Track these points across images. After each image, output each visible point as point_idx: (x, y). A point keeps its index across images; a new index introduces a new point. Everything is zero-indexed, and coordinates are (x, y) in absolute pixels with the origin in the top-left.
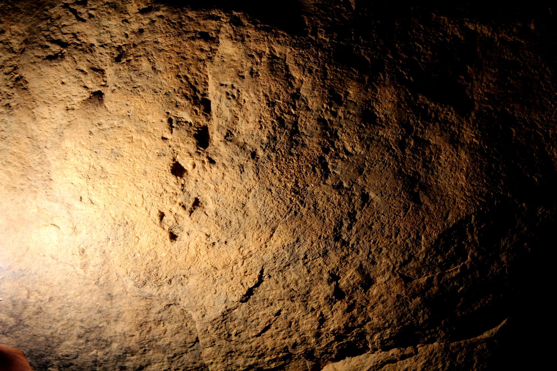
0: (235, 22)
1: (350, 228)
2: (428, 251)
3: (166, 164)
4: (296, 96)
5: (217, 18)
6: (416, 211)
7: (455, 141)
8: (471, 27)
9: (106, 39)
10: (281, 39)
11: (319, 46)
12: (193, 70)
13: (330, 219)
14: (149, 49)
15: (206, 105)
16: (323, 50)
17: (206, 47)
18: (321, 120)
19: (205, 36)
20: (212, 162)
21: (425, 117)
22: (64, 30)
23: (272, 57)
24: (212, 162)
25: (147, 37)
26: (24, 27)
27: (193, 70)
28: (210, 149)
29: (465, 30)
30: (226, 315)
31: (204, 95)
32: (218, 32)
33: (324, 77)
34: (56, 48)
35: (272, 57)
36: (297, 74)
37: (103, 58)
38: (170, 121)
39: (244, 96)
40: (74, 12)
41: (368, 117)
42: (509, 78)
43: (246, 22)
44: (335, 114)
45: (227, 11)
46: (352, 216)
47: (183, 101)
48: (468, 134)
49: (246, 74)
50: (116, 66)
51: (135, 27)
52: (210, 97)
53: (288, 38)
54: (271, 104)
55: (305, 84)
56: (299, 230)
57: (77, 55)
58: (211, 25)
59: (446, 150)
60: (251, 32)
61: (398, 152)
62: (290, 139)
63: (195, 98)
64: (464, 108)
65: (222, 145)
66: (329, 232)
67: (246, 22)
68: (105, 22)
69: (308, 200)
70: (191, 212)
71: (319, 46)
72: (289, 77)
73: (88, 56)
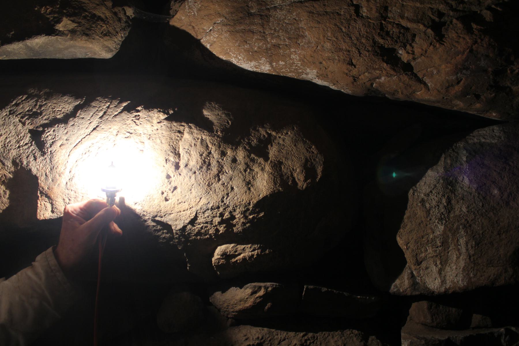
0: (190, 128)
1: (227, 198)
2: (253, 207)
3: (164, 175)
4: (210, 153)
5: (184, 126)
6: (249, 194)
7: (263, 170)
8: (269, 132)
9: (146, 132)
10: (205, 134)
11: (218, 136)
12: (175, 143)
13: (220, 196)
14: (160, 135)
15: (179, 155)
16: (220, 138)
17: (179, 135)
18: (218, 162)
19: (179, 132)
20: (180, 174)
21: (253, 160)
22: (131, 128)
23: (202, 139)
24: (180, 174)
25: (159, 131)
26: (118, 127)
27: (175, 143)
28: (180, 170)
29: (267, 133)
30: (185, 227)
31: (178, 152)
32: (184, 130)
33: (220, 147)
34: (128, 134)
35: (202, 139)
36: (210, 146)
37: (145, 138)
38: (166, 160)
39: (192, 152)
40: (135, 122)
41: (234, 160)
42: (188, 268)
43: (193, 127)
44: (223, 160)
45: (187, 123)
46: (228, 194)
47: (171, 154)
48: (268, 168)
49: (193, 145)
50: (149, 141)
51: (156, 128)
52: (180, 153)
53: (208, 133)
54: (201, 155)
55: (213, 149)
56: (209, 199)
57: (135, 136)
58: (181, 128)
59: (260, 173)
60: (195, 131)
61: (244, 173)
62: (207, 167)
63: (175, 153)
64: (266, 159)
65: (184, 169)
66: (220, 200)
67: (193, 127)
68: (145, 126)
69: (213, 189)
70: (173, 192)
71: (218, 136)
72: (207, 146)
73: (139, 137)
